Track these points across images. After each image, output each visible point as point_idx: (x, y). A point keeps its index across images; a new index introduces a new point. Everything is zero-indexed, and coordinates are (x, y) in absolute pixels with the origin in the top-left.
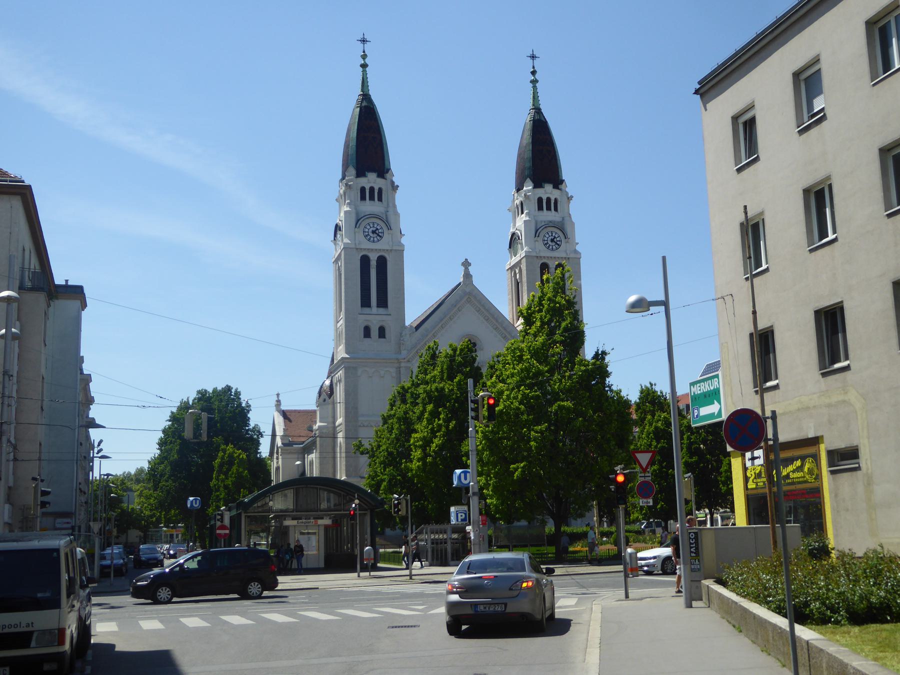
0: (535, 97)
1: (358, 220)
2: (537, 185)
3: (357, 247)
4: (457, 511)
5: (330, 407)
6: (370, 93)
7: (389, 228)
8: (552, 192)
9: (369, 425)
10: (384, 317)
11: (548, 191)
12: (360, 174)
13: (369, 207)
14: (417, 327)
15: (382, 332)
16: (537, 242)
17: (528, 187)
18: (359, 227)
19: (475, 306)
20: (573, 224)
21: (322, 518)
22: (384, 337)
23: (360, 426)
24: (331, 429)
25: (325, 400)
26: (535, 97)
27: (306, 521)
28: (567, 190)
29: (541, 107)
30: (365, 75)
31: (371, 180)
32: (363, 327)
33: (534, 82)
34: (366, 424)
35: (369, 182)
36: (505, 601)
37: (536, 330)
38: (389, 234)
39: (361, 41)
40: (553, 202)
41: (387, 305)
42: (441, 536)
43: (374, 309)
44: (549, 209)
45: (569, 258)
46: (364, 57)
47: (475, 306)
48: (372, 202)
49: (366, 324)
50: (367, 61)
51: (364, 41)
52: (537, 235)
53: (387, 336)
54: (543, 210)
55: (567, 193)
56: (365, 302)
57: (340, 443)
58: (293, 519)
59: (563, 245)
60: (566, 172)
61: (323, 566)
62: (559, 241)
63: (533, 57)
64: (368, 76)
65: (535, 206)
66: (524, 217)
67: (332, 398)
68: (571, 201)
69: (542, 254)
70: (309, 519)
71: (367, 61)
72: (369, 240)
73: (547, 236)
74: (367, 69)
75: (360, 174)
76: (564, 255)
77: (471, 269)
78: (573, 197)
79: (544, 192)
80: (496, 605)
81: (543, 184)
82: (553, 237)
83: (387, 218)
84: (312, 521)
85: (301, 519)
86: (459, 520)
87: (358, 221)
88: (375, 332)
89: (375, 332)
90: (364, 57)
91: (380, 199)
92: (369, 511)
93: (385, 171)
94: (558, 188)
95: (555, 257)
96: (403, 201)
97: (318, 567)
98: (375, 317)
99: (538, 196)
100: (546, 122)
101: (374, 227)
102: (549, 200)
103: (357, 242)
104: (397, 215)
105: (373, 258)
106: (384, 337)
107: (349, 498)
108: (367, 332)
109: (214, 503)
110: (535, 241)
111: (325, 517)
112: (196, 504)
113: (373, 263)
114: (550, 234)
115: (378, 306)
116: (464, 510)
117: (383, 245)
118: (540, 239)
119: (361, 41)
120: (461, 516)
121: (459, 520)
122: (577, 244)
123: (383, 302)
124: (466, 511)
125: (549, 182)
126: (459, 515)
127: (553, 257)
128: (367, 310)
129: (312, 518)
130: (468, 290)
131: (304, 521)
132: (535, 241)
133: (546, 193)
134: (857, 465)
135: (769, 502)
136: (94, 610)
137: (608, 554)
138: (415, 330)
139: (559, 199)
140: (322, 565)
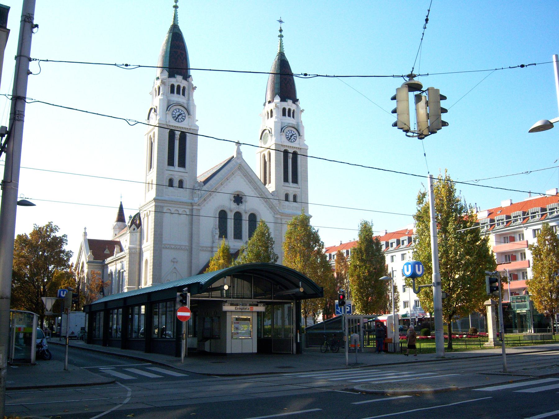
0: (281, 46)
1: (169, 106)
2: (283, 99)
3: (168, 124)
5: (138, 234)
6: (179, 25)
7: (189, 114)
8: (181, 81)
9: (170, 247)
10: (296, 190)
11: (289, 104)
12: (171, 75)
13: (176, 98)
14: (206, 182)
15: (181, 184)
16: (282, 136)
17: (277, 99)
18: (169, 110)
20: (303, 127)
21: (257, 305)
23: (164, 248)
24: (138, 250)
25: (134, 229)
26: (281, 46)
27: (243, 307)
28: (193, 82)
29: (284, 52)
30: (176, 13)
31: (178, 80)
32: (168, 179)
33: (281, 36)
35: (177, 82)
38: (189, 118)
39: (279, 21)
40: (181, 89)
43: (176, 168)
44: (289, 116)
45: (301, 148)
46: (281, 31)
48: (178, 95)
49: (171, 177)
50: (283, 33)
51: (281, 21)
52: (168, 109)
55: (192, 85)
56: (171, 163)
57: (147, 261)
58: (232, 305)
59: (298, 139)
62: (184, 116)
63: (281, 21)
64: (178, 14)
65: (281, 112)
66: (274, 119)
68: (195, 90)
69: (285, 144)
70: (246, 305)
71: (283, 33)
73: (288, 133)
74: (178, 9)
75: (171, 75)
76: (298, 146)
78: (196, 87)
81: (176, 75)
82: (292, 134)
83: (188, 106)
84: (248, 307)
87: (282, 129)
90: (281, 31)
91: (184, 94)
93: (188, 77)
94: (295, 104)
95: (293, 147)
96: (197, 96)
98: (177, 172)
100: (288, 62)
101: (179, 112)
102: (289, 110)
103: (168, 121)
104: (194, 106)
107: (279, 287)
108: (171, 183)
110: (281, 135)
112: (63, 294)
114: (178, 111)
115: (179, 166)
117: (184, 125)
118: (284, 134)
119: (279, 21)
122: (305, 140)
123: (182, 164)
125: (290, 99)
127: (292, 146)
128: (171, 168)
130: (239, 161)
132: (281, 135)
133: (288, 105)
137: (419, 347)
138: (203, 184)
139: (296, 110)
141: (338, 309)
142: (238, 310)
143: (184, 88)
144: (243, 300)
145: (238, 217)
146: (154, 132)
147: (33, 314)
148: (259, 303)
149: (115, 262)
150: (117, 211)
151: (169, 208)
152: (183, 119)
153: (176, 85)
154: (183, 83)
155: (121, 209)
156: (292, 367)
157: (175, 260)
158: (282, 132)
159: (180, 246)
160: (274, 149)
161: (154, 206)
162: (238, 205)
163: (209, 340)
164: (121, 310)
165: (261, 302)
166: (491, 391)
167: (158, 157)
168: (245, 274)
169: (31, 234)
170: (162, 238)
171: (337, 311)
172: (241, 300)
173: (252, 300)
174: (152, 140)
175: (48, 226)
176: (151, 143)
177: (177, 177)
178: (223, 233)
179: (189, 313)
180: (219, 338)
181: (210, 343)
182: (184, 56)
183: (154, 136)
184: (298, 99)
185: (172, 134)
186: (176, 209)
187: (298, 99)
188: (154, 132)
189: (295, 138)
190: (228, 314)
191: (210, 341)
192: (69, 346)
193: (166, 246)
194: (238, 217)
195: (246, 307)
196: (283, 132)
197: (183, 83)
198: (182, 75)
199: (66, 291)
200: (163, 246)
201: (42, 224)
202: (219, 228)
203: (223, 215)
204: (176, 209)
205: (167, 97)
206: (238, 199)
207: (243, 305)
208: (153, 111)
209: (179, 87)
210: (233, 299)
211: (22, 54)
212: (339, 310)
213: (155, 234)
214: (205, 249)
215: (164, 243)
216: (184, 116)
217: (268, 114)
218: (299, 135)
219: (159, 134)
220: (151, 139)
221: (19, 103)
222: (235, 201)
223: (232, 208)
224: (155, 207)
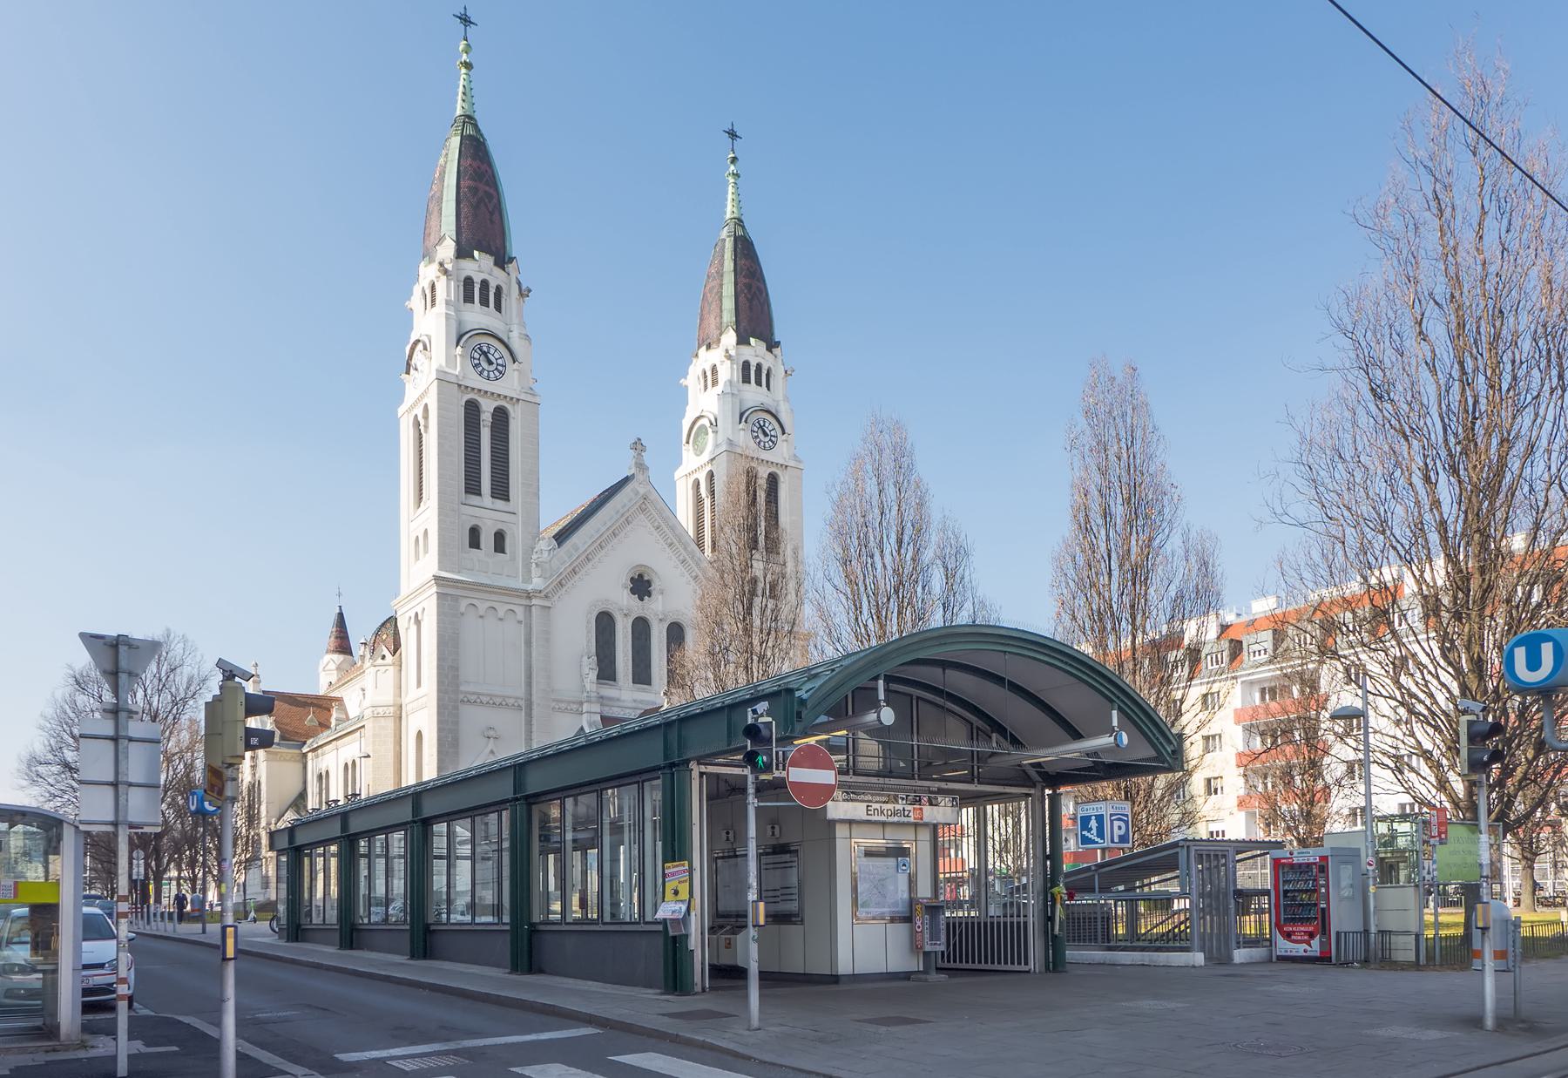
4: (1111, 815)
22: (503, 551)
34: (485, 699)
40: (753, 370)
41: (480, 490)
53: (507, 549)
54: (750, 383)
56: (472, 487)
60: (517, 244)
62: (502, 366)
67: (398, 652)
72: (481, 374)
77: (647, 458)
79: (753, 353)
80: (628, 920)
88: (487, 540)
89: (487, 540)
98: (487, 512)
99: (745, 359)
105: (763, 473)
106: (503, 551)
113: (486, 418)
120: (1120, 828)
121: (1116, 840)
123: (501, 490)
124: (1127, 816)
125: (760, 337)
126: (1116, 824)
128: (474, 499)
134: (850, 713)
136: (1456, 925)
141: (1090, 830)
142: (876, 818)
143: (499, 289)
145: (641, 628)
146: (426, 405)
149: (334, 743)
150: (332, 618)
151: (475, 601)
152: (500, 373)
153: (477, 279)
154: (496, 277)
155: (341, 621)
157: (491, 733)
158: (743, 423)
159: (504, 697)
161: (435, 596)
162: (641, 599)
164: (397, 837)
167: (440, 477)
170: (458, 676)
174: (422, 428)
176: (417, 435)
177: (489, 523)
178: (606, 672)
182: (495, 201)
183: (426, 417)
184: (779, 342)
185: (472, 409)
186: (489, 604)
187: (779, 342)
188: (426, 405)
189: (773, 439)
190: (841, 831)
193: (469, 696)
194: (641, 628)
196: (746, 422)
197: (496, 277)
198: (491, 254)
200: (461, 697)
202: (597, 655)
203: (605, 623)
204: (489, 604)
205: (457, 311)
206: (641, 586)
208: (420, 346)
209: (485, 284)
210: (855, 779)
211: (122, 733)
212: (1094, 831)
213: (440, 667)
214: (563, 706)
215: (462, 688)
216: (502, 366)
217: (705, 377)
218: (784, 433)
219: (440, 408)
220: (417, 424)
221: (109, 667)
222: (633, 591)
223: (624, 604)
224: (438, 599)
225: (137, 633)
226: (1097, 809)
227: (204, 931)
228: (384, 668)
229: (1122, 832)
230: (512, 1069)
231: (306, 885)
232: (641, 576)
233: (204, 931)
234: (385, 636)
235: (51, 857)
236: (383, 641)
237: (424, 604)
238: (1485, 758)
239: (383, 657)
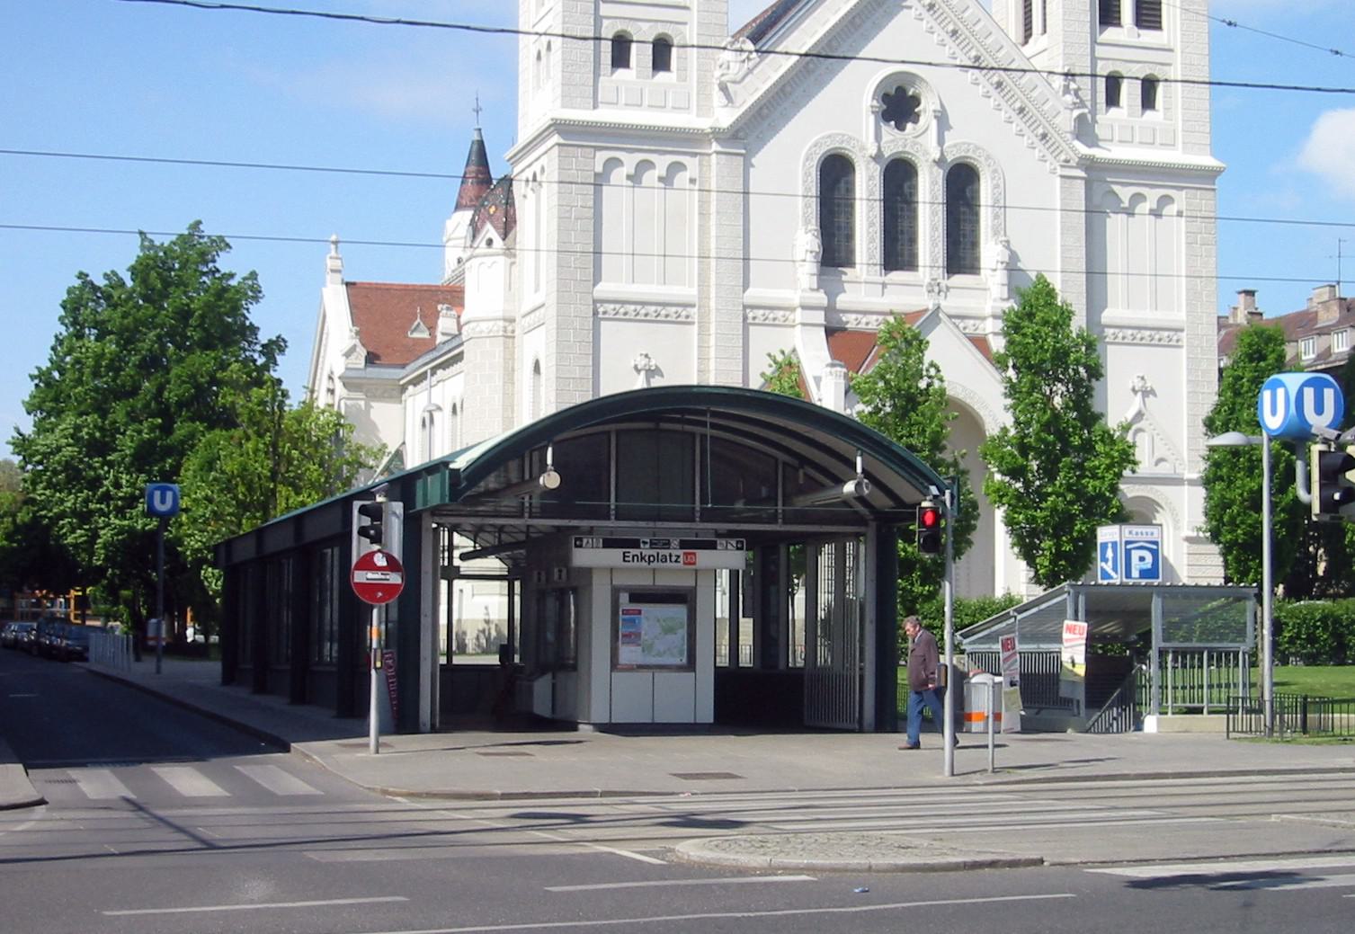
4: (1127, 543)
19: (796, 79)
21: (711, 546)
27: (654, 552)
36: (957, 780)
37: (358, 476)
42: (65, 642)
47: (796, 79)
58: (609, 544)
61: (712, 721)
70: (667, 545)
84: (675, 552)
85: (635, 544)
86: (1135, 574)
92: (873, 525)
97: (649, 721)
107: (805, 474)
109: (326, 414)
111: (721, 542)
112: (163, 501)
116: (1150, 538)
120: (1142, 559)
121: (1135, 574)
126: (1135, 555)
129: (675, 543)
131: (647, 552)
135: (573, 615)
140: (707, 714)
141: (1106, 561)
144: (659, 524)
145: (899, 175)
147: (694, 554)
148: (719, 535)
156: (675, 775)
160: (521, 36)
163: (549, 677)
165: (731, 534)
166: (215, 757)
168: (664, 426)
169: (133, 270)
171: (1102, 569)
172: (651, 524)
173: (693, 525)
175: (185, 240)
179: (356, 580)
180: (575, 668)
181: (554, 686)
191: (554, 678)
192: (987, 746)
194: (899, 175)
195: (666, 552)
199: (170, 489)
201: (166, 232)
207: (653, 545)
212: (1110, 563)
225: (24, 409)
226: (1137, 534)
227: (158, 671)
228: (488, 260)
229: (1148, 564)
230: (237, 767)
231: (517, 599)
232: (901, 91)
233: (158, 671)
234: (492, 210)
235: (939, 108)
236: (491, 216)
237: (544, 160)
238: (1337, 496)
239: (490, 242)
